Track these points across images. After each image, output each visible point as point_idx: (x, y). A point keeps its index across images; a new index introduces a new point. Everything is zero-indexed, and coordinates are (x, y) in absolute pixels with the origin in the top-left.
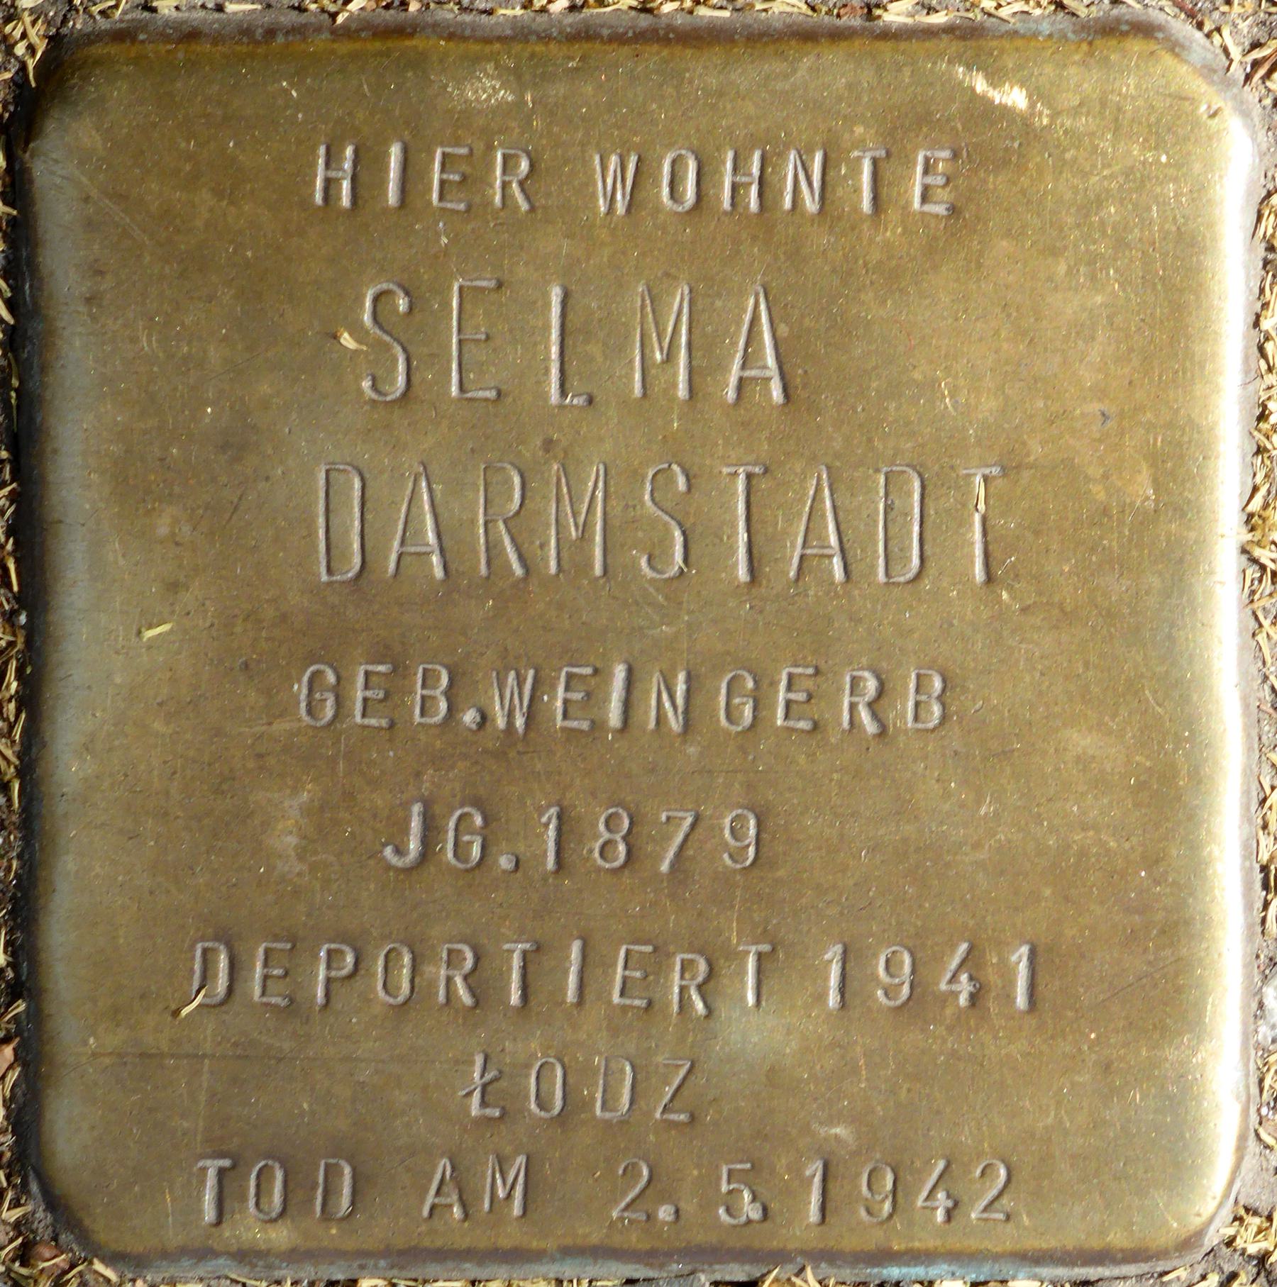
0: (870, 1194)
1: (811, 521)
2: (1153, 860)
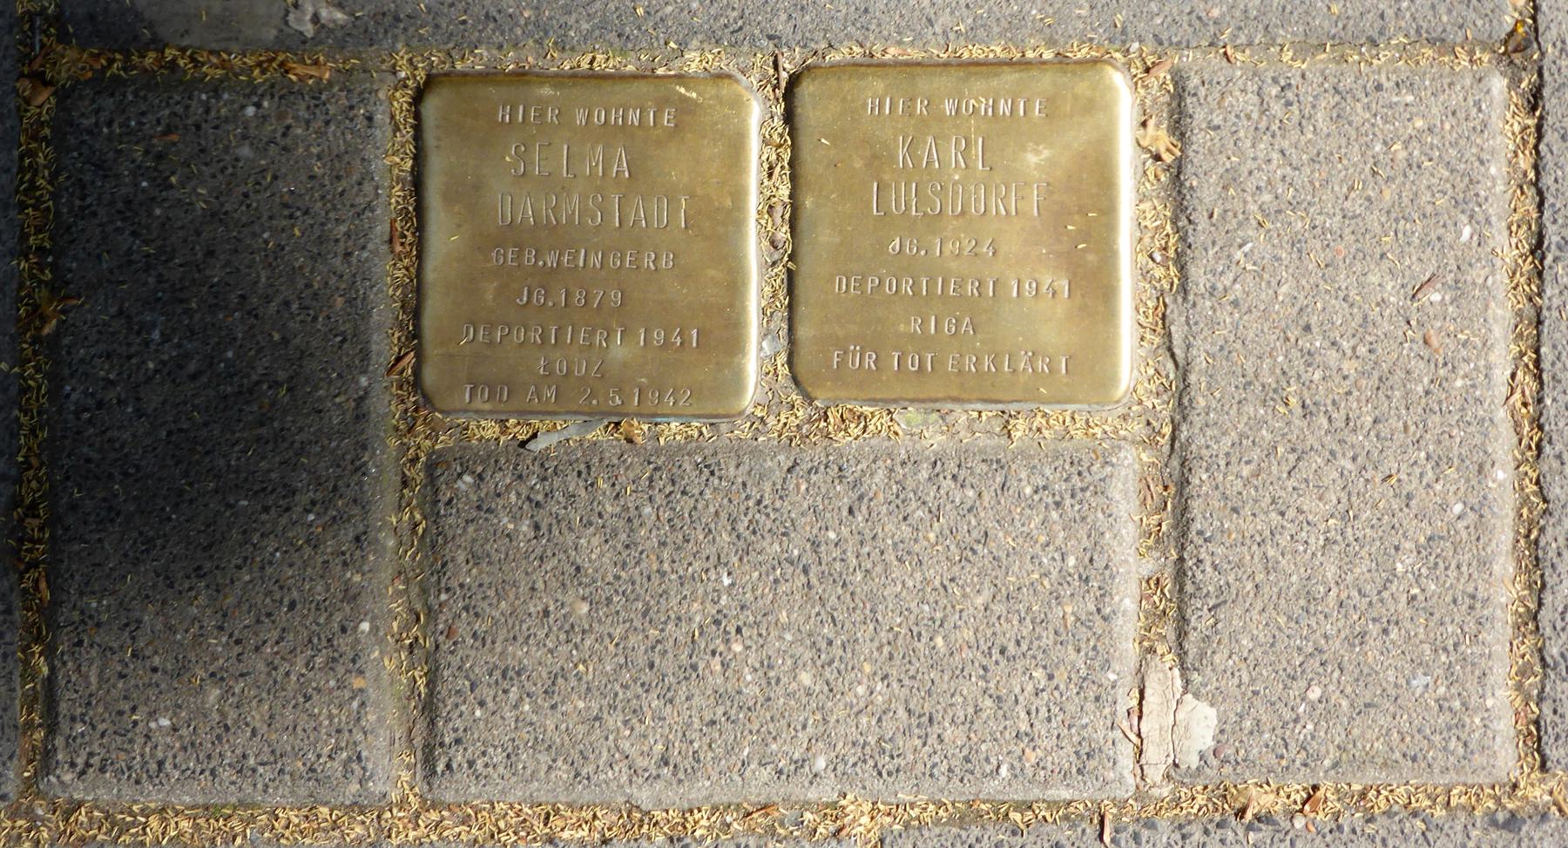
0: (652, 397)
1: (638, 212)
2: (731, 306)
